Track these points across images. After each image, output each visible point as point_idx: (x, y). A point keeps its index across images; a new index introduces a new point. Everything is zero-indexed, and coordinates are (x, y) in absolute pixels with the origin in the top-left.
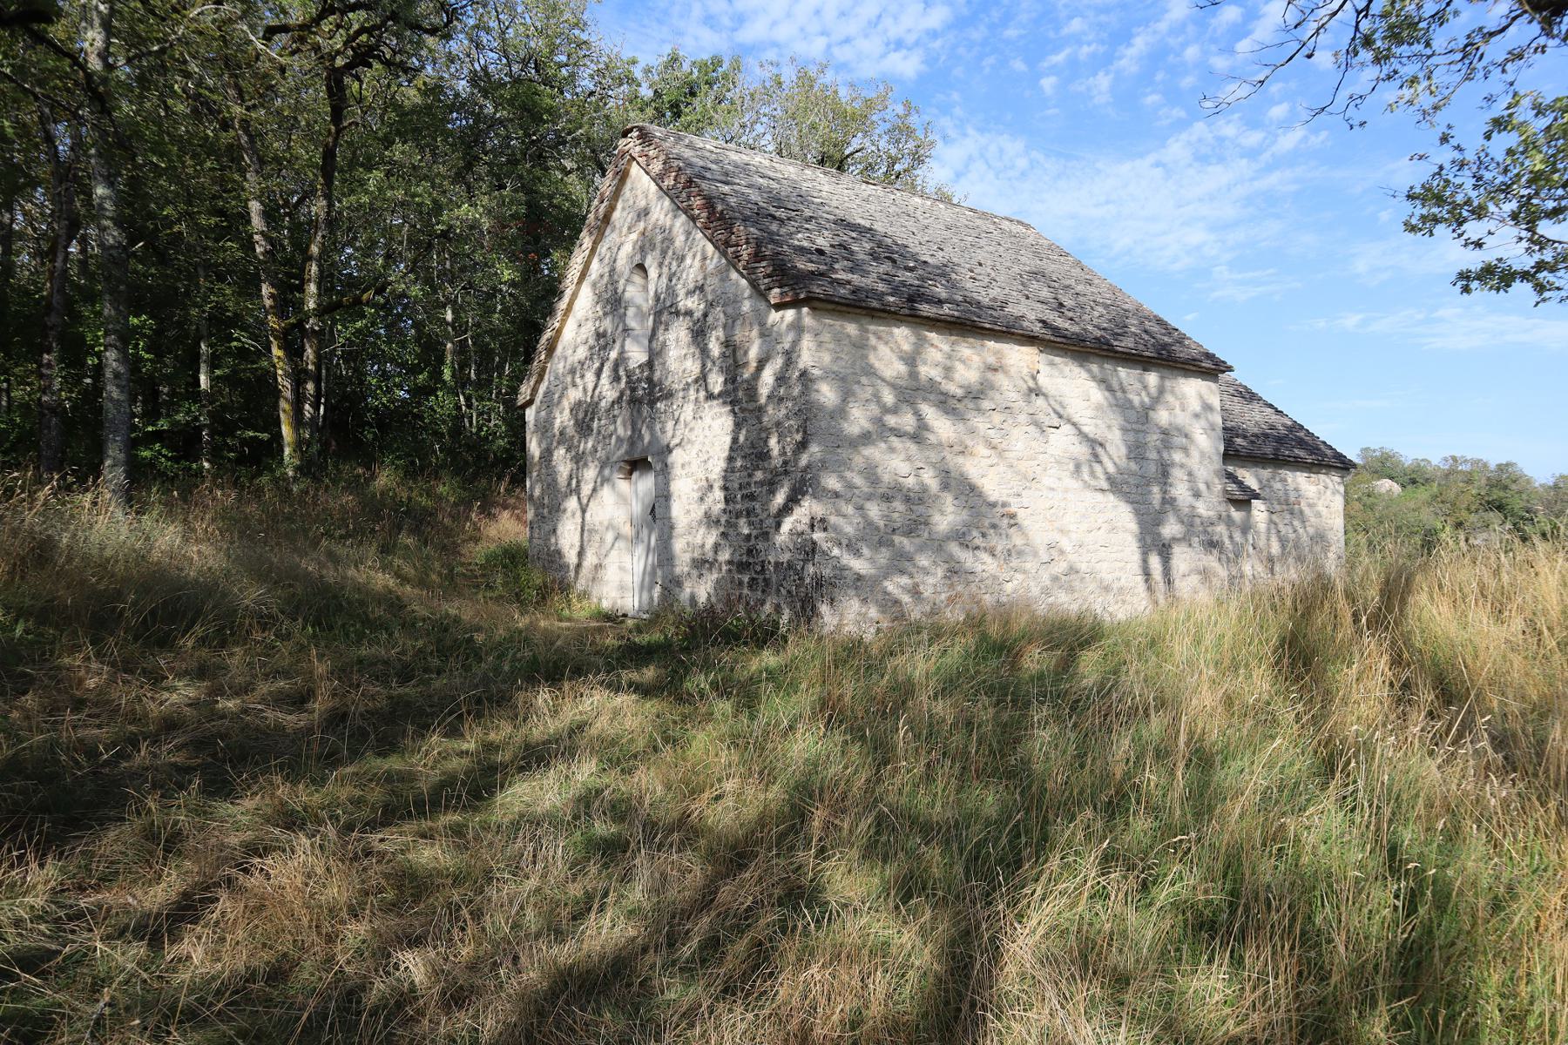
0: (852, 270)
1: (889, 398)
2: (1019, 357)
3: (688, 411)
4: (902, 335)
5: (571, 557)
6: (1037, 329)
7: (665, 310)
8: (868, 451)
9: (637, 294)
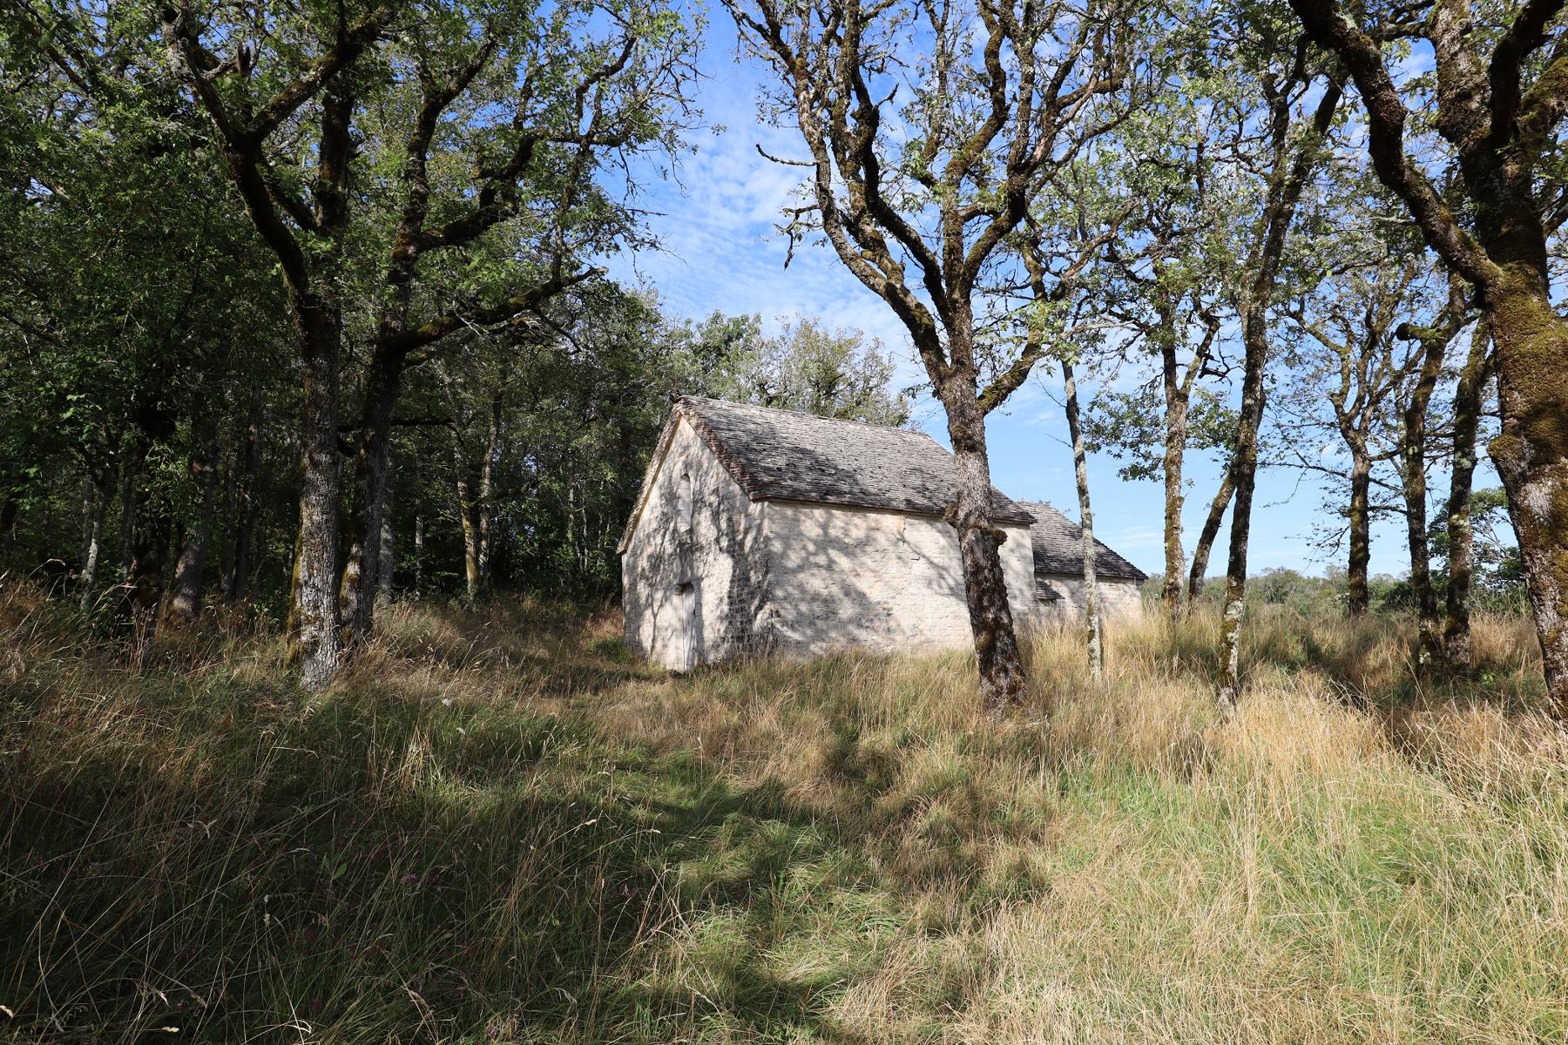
0: (795, 480)
1: (811, 547)
2: (890, 522)
3: (711, 557)
4: (819, 513)
5: (647, 644)
6: (902, 506)
7: (698, 502)
8: (801, 576)
9: (684, 491)
